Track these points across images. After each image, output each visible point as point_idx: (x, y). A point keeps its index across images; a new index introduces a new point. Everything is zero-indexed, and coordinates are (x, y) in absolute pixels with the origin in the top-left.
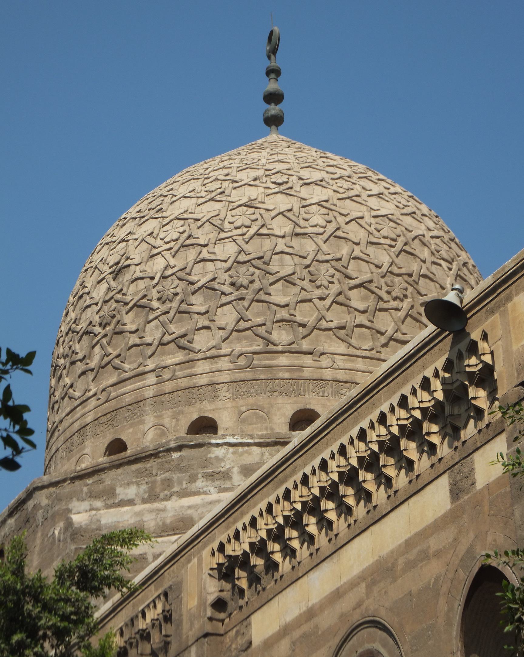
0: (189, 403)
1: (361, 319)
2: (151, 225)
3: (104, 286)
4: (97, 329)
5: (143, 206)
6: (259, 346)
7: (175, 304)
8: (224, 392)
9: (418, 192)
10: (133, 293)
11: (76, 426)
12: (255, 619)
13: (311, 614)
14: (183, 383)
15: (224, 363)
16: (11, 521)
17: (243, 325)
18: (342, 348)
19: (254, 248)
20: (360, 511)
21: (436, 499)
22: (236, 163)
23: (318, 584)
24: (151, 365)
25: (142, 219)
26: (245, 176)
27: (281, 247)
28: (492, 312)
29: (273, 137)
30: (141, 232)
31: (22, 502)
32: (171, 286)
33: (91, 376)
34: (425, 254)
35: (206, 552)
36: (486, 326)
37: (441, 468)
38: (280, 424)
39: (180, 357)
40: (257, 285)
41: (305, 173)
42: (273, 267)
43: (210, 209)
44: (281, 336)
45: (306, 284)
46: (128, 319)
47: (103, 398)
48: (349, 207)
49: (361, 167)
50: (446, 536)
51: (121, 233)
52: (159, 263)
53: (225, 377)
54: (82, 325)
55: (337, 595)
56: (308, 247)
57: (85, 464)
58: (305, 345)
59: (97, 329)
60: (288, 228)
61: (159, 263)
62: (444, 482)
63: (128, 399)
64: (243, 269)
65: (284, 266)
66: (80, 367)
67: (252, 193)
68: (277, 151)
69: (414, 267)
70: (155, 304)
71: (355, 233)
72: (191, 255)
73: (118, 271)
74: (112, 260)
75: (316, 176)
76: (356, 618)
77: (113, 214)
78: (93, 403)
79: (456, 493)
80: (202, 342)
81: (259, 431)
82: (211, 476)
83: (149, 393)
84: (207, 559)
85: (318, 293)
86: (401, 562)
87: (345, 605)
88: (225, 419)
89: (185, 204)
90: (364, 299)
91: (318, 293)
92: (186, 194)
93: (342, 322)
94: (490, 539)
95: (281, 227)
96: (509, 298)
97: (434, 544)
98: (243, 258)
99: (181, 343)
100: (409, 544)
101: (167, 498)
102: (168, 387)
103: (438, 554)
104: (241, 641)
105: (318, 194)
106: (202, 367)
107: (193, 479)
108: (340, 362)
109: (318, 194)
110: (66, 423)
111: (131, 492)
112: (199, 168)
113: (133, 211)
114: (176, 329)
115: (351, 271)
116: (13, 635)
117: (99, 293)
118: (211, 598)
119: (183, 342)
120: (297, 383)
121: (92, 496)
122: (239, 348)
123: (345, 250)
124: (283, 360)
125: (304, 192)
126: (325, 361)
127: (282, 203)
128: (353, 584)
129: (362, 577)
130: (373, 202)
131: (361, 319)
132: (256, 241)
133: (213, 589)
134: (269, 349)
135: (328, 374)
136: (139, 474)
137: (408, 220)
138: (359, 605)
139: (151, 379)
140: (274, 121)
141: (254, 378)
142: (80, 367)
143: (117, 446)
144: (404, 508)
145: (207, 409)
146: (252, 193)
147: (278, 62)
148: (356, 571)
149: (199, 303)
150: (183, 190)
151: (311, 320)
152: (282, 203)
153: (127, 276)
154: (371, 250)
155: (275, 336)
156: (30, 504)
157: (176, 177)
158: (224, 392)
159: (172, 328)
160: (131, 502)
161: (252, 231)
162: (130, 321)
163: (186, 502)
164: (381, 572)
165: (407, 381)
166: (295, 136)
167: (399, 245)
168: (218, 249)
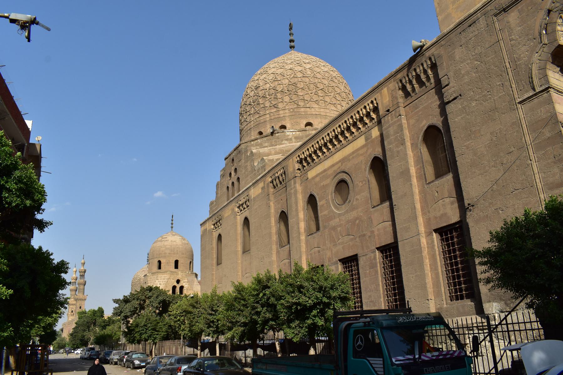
0: (278, 122)
1: (321, 98)
2: (264, 76)
3: (253, 92)
4: (252, 103)
5: (262, 70)
6: (296, 106)
7: (273, 96)
8: (288, 119)
9: (332, 65)
10: (261, 93)
11: (249, 128)
12: (309, 173)
13: (325, 171)
14: (277, 116)
15: (287, 111)
16: (235, 152)
17: (291, 101)
18: (317, 107)
19: (293, 81)
20: (338, 146)
21: (361, 141)
22: (286, 58)
23: (327, 164)
24: (267, 112)
25: (261, 74)
26: (289, 62)
27: (300, 80)
28: (378, 93)
29: (293, 51)
30: (262, 78)
31: (237, 148)
32: (272, 91)
33: (251, 115)
34: (336, 81)
35: (294, 158)
36: (376, 97)
37: (362, 133)
38: (303, 126)
39: (275, 110)
40: (294, 90)
41: (304, 60)
42: (298, 85)
43: (279, 71)
44: (301, 104)
45: (307, 90)
46: (260, 100)
47: (255, 121)
48: (316, 69)
49: (318, 59)
50: (364, 150)
51: (256, 78)
52: (268, 85)
53: (287, 115)
54: (248, 103)
55: (333, 166)
56: (307, 80)
57: (253, 138)
58: (308, 106)
59: (252, 103)
60: (302, 75)
61: (268, 85)
62: (363, 137)
63: (262, 121)
64: (290, 86)
65: (301, 85)
66: (248, 113)
67: (291, 66)
68: (294, 55)
69: (334, 84)
70: (268, 96)
71: (318, 76)
72: (276, 83)
73: (257, 88)
74: (255, 85)
75: (307, 61)
76: (338, 171)
77: (253, 73)
78: (252, 122)
79: (366, 139)
80: (280, 106)
81: (298, 128)
82: (287, 140)
83: (268, 119)
84: (296, 159)
85: (310, 92)
86: (351, 157)
87: (335, 168)
88: (288, 126)
89: (273, 70)
90: (322, 93)
91: (310, 92)
92: (273, 67)
93: (317, 99)
94: (376, 150)
95: (299, 75)
96: (382, 89)
97: (361, 152)
98: (290, 83)
99: (275, 106)
100: (353, 153)
101: (276, 145)
102: (272, 118)
103: (362, 155)
104: (305, 178)
105: (308, 66)
106: (281, 112)
107: (282, 141)
108: (317, 109)
109: (308, 66)
110: (246, 128)
111: (266, 144)
112: (276, 60)
113: (259, 72)
114: (274, 103)
115: (318, 86)
116: (30, 241)
117: (252, 94)
118: (297, 168)
119: (276, 106)
120: (306, 115)
121: (256, 145)
122: (291, 107)
123: (316, 81)
124: (302, 110)
125: (304, 65)
126: (313, 110)
127: (300, 68)
128: (337, 163)
129: (340, 161)
130: (322, 68)
131: (321, 98)
132: (293, 79)
133: (297, 166)
134: (298, 106)
135: (314, 113)
136: (268, 140)
137: (331, 72)
138: (339, 168)
139: (268, 116)
140: (292, 47)
141: (295, 115)
142: (248, 113)
143: (261, 133)
144: (351, 144)
145: (284, 123)
146: (291, 66)
147: (292, 31)
148: (338, 160)
149: (279, 95)
150: (272, 66)
151: (309, 99)
152: (300, 68)
153: (260, 89)
154: (323, 80)
155: (300, 103)
156: (240, 147)
157: (269, 63)
158: (288, 119)
159: (272, 102)
160: (267, 147)
161: (292, 76)
162: (261, 101)
163: (281, 146)
164: (343, 161)
165: (353, 111)
166: (299, 51)
167: (330, 79)
168: (283, 81)
